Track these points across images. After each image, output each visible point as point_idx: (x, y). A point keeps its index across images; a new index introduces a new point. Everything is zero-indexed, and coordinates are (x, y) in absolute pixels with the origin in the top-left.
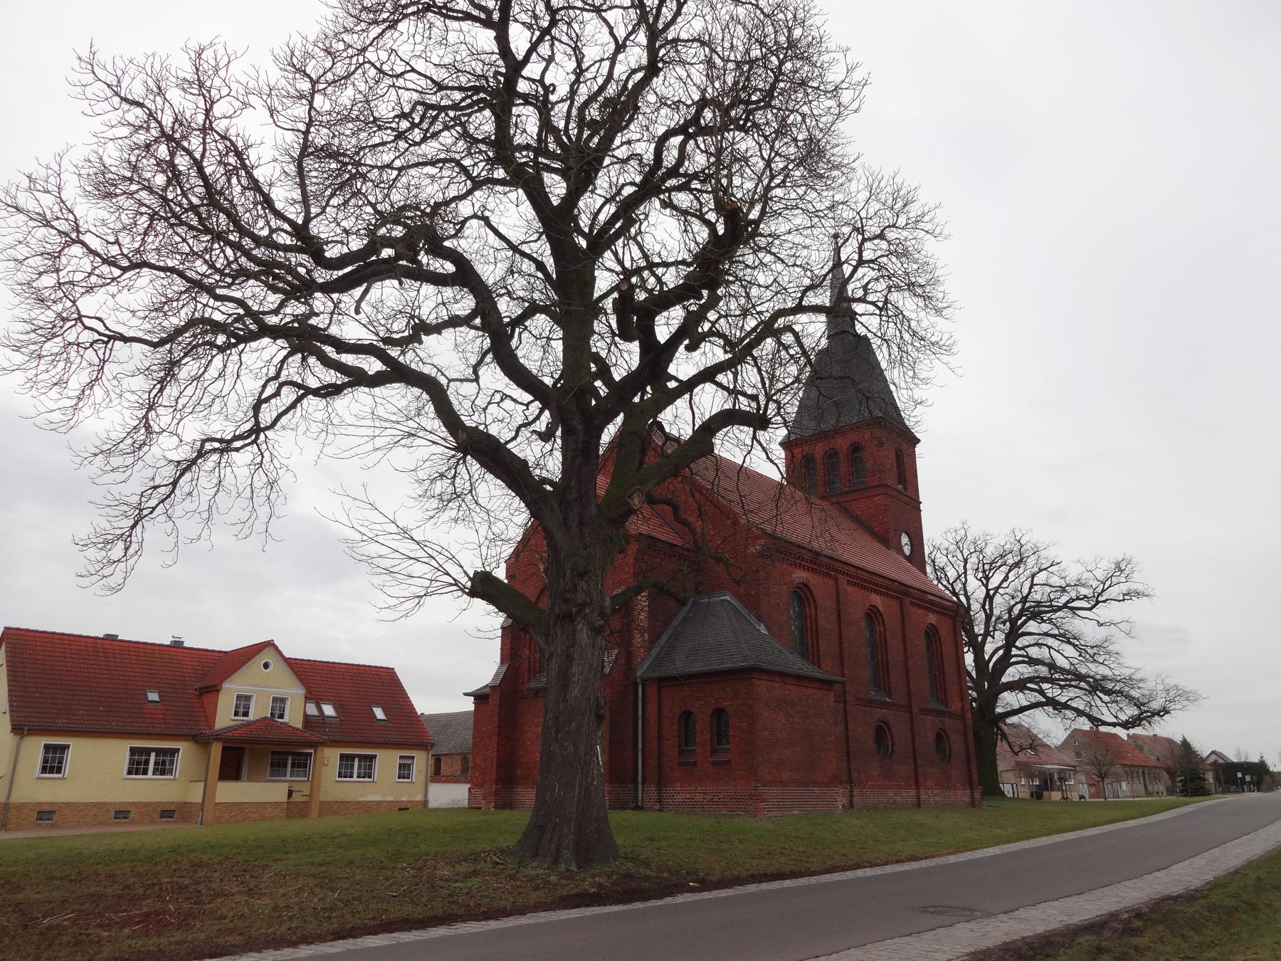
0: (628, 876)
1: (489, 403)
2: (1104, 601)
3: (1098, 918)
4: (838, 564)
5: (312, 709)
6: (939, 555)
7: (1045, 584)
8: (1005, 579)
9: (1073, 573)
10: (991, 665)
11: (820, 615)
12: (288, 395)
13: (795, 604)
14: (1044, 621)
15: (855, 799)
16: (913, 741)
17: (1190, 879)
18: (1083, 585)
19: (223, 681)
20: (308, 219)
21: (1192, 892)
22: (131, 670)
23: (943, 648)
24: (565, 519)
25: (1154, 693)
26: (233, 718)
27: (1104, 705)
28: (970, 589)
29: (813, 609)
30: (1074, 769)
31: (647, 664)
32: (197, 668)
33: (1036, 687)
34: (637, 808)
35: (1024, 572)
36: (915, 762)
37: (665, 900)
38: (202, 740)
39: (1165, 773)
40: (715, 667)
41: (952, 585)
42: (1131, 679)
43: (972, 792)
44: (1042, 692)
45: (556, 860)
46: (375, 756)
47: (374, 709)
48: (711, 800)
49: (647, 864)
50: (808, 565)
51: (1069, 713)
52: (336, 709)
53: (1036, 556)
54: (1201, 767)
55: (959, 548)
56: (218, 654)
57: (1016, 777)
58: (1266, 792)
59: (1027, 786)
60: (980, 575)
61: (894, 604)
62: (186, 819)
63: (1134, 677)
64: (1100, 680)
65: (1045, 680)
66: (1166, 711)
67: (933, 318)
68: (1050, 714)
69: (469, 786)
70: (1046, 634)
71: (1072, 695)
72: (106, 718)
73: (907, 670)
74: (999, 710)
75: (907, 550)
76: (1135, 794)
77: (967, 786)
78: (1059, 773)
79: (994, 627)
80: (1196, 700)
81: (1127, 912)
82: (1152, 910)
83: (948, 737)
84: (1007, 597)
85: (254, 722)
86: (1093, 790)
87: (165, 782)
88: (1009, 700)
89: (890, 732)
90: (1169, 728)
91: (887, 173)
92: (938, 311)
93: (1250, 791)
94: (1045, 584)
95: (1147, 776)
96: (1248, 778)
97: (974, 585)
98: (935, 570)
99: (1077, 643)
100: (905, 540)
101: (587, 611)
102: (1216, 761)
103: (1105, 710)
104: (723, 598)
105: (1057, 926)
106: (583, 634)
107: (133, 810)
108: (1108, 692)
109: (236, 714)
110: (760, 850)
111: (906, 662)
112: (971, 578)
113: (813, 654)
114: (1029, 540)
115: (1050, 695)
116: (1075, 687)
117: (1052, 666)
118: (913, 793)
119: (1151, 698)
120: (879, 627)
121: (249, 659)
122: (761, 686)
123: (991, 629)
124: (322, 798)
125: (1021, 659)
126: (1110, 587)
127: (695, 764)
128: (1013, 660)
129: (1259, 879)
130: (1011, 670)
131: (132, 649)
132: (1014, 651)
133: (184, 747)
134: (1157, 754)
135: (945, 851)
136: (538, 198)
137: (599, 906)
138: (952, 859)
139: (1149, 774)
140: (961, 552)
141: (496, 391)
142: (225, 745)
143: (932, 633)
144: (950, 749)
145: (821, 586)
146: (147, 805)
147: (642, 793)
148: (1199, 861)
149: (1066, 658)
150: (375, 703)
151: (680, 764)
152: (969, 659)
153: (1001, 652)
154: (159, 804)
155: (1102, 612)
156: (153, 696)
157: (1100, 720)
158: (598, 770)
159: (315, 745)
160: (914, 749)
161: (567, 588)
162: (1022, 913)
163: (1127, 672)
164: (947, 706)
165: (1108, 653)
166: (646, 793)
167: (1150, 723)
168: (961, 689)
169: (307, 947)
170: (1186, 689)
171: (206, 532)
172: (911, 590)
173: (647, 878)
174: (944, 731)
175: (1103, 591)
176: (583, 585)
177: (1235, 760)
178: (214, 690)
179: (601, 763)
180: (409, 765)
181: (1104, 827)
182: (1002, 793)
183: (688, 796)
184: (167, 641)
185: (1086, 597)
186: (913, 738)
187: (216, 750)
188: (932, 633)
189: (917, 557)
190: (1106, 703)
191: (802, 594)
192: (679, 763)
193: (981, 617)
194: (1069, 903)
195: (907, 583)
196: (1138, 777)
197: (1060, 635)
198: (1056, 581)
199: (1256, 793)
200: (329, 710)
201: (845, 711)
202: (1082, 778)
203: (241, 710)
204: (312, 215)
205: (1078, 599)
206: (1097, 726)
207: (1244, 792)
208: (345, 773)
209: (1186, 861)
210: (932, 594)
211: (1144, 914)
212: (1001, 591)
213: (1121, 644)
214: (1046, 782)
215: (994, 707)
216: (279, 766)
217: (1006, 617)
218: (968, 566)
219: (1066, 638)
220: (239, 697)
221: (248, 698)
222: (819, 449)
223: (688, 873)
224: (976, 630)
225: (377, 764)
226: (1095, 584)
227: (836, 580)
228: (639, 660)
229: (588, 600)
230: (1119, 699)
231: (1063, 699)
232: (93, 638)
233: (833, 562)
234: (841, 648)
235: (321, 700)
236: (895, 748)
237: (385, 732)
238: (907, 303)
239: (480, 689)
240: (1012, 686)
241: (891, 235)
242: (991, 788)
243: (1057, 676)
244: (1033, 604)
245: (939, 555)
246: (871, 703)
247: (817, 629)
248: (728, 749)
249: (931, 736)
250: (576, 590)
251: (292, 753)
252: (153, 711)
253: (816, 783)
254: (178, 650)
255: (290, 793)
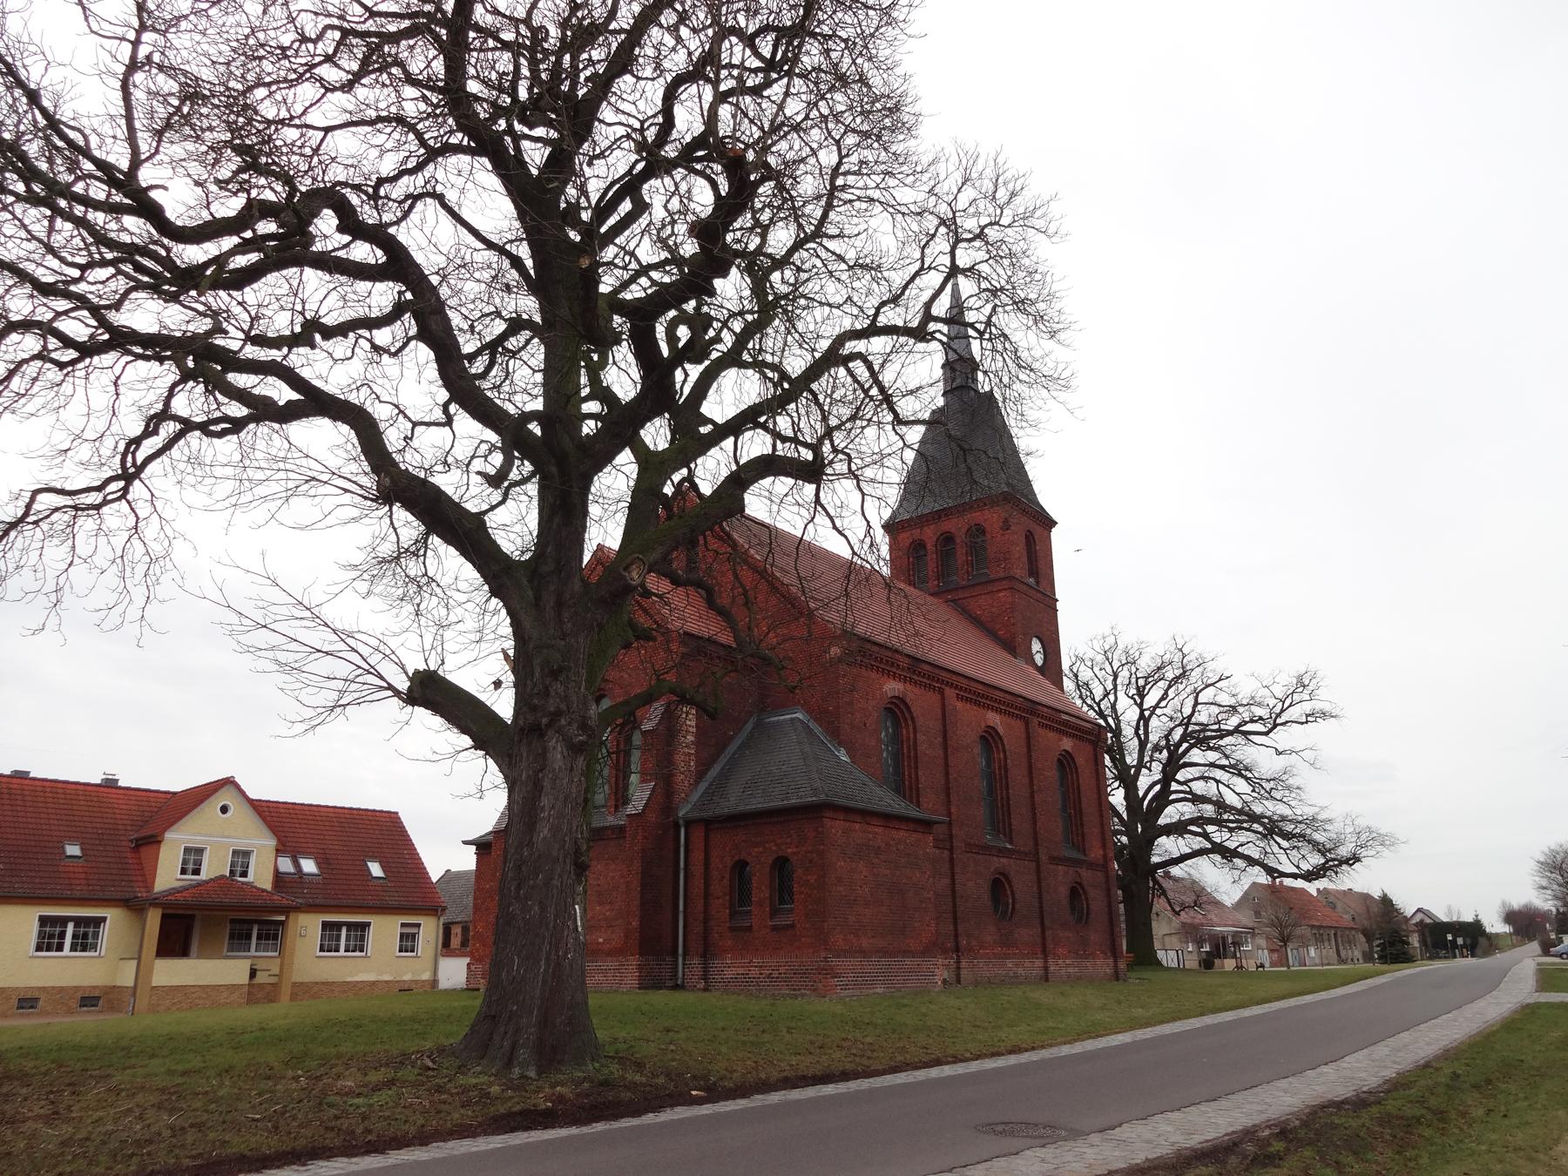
0: (606, 1084)
1: (473, 457)
2: (1283, 724)
3: (1227, 1138)
4: (944, 674)
5: (286, 865)
6: (1083, 668)
7: (1212, 704)
8: (1162, 699)
9: (1245, 688)
10: (1146, 803)
11: (921, 737)
12: (169, 428)
13: (889, 724)
14: (1210, 748)
15: (964, 973)
16: (1040, 898)
17: (1363, 1075)
18: (1259, 705)
19: (165, 830)
20: (136, 163)
21: (1364, 1095)
22: (46, 816)
23: (1081, 780)
24: (538, 598)
25: (1343, 836)
26: (179, 876)
27: (1282, 851)
28: (1120, 707)
29: (911, 730)
30: (1253, 932)
31: (695, 797)
32: (134, 813)
33: (1199, 830)
34: (676, 987)
35: (1184, 688)
36: (1042, 924)
37: (644, 1118)
38: (135, 906)
39: (1361, 936)
40: (777, 804)
41: (1098, 705)
42: (1314, 819)
43: (1115, 961)
44: (1206, 836)
45: (509, 1063)
46: (369, 924)
47: (369, 864)
48: (769, 976)
49: (640, 1066)
50: (889, 668)
51: (1238, 861)
52: (318, 864)
53: (1200, 669)
54: (1405, 927)
55: (1108, 659)
56: (163, 796)
57: (1181, 942)
58: (1482, 958)
59: (1195, 954)
60: (1133, 691)
61: (1018, 725)
62: (113, 1007)
63: (1320, 817)
64: (1277, 821)
65: (1211, 821)
66: (1354, 859)
67: (1049, 345)
68: (1217, 863)
69: (467, 960)
70: (1213, 765)
71: (1243, 839)
72: (8, 879)
73: (1034, 809)
74: (1155, 859)
75: (1039, 659)
76: (1325, 961)
77: (1109, 954)
78: (1233, 936)
79: (1151, 757)
80: (1393, 844)
81: (1269, 1127)
82: (1305, 1124)
83: (1085, 892)
84: (1164, 719)
85: (207, 882)
86: (1275, 956)
87: (87, 960)
88: (1167, 846)
89: (1011, 887)
90: (1363, 880)
91: (987, 151)
92: (1053, 334)
93: (1463, 956)
94: (1212, 704)
95: (1340, 940)
96: (1460, 941)
97: (1124, 703)
98: (1078, 686)
99: (1250, 775)
100: (1036, 646)
101: (563, 722)
102: (1422, 921)
103: (1283, 858)
104: (794, 716)
105: (1164, 1152)
106: (557, 753)
107: (43, 997)
108: (1287, 836)
109: (183, 871)
110: (812, 1043)
111: (1032, 797)
112: (1121, 694)
113: (911, 788)
114: (1194, 649)
115: (1218, 840)
116: (1248, 830)
117: (1221, 805)
118: (1039, 963)
119: (1338, 844)
120: (998, 752)
121: (202, 801)
122: (835, 827)
123: (1147, 759)
124: (297, 978)
125: (1182, 795)
126: (1290, 706)
127: (750, 929)
128: (1173, 797)
129: (1456, 1076)
130: (1169, 810)
131: (48, 790)
132: (1174, 786)
133: (112, 915)
134: (1352, 913)
135: (1060, 1040)
136: (510, 170)
137: (546, 1128)
138: (1066, 1050)
139: (1342, 937)
140: (1111, 664)
141: (482, 441)
142: (166, 911)
143: (1066, 762)
144: (1088, 908)
145: (922, 702)
146: (61, 989)
147: (684, 968)
148: (1382, 1050)
149: (1238, 794)
150: (303, 853)
151: (732, 929)
152: (1117, 798)
153: (1158, 788)
154: (77, 988)
155: (1281, 737)
156: (73, 850)
157: (1277, 871)
158: (576, 939)
159: (287, 910)
160: (1041, 907)
161: (535, 691)
162: (1125, 1132)
163: (1309, 811)
164: (1085, 855)
165: (1289, 788)
166: (687, 967)
167: (1336, 873)
168: (1103, 833)
169: (326, 1163)
170: (1382, 832)
171: (53, 620)
172: (1040, 707)
173: (628, 1087)
174: (1079, 884)
175: (1282, 711)
176: (558, 687)
177: (1445, 919)
178: (155, 841)
179: (580, 929)
180: (414, 935)
181: (1272, 1005)
182: (1159, 963)
183: (741, 971)
184: (96, 779)
185: (1261, 718)
186: (1040, 893)
187: (154, 919)
188: (1066, 762)
189: (1052, 668)
190: (1285, 850)
191: (897, 710)
192: (729, 928)
193: (1132, 745)
194: (1193, 1115)
195: (1035, 699)
196: (1329, 940)
197: (1231, 766)
198: (1225, 699)
199: (1470, 958)
200: (309, 866)
201: (952, 860)
202: (1262, 942)
203: (191, 866)
204: (143, 157)
205: (1252, 721)
206: (1274, 878)
207: (1455, 957)
208: (329, 944)
209: (1365, 1051)
210: (1067, 713)
211: (1290, 1131)
212: (1158, 711)
213: (1302, 776)
214: (1217, 947)
215: (1149, 855)
216: (240, 937)
217: (1163, 743)
218: (1119, 681)
219: (1239, 770)
220: (187, 850)
221: (200, 851)
222: (930, 534)
223: (694, 1077)
224: (1129, 760)
225: (372, 934)
226: (1272, 702)
227: (941, 692)
228: (683, 795)
229: (563, 707)
230: (1300, 844)
231: (1232, 845)
232: (51, 781)
233: (937, 671)
234: (947, 781)
235: (299, 853)
236: (1017, 906)
237: (382, 893)
238: (1009, 322)
239: (484, 836)
240: (1169, 830)
241: (992, 233)
242: (1144, 956)
243: (1225, 817)
244: (1197, 728)
245: (1083, 668)
246: (986, 849)
247: (916, 754)
248: (792, 909)
249: (1064, 891)
250: (548, 695)
251: (256, 921)
252: (71, 869)
253: (906, 953)
254: (110, 790)
255: (253, 973)
